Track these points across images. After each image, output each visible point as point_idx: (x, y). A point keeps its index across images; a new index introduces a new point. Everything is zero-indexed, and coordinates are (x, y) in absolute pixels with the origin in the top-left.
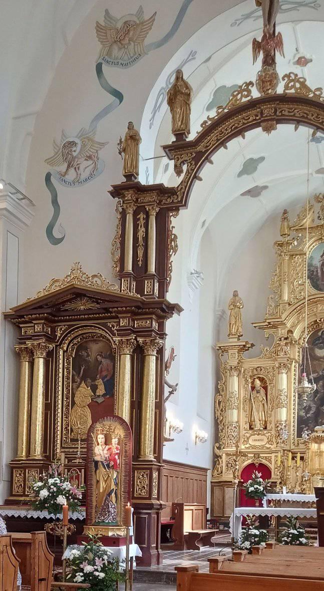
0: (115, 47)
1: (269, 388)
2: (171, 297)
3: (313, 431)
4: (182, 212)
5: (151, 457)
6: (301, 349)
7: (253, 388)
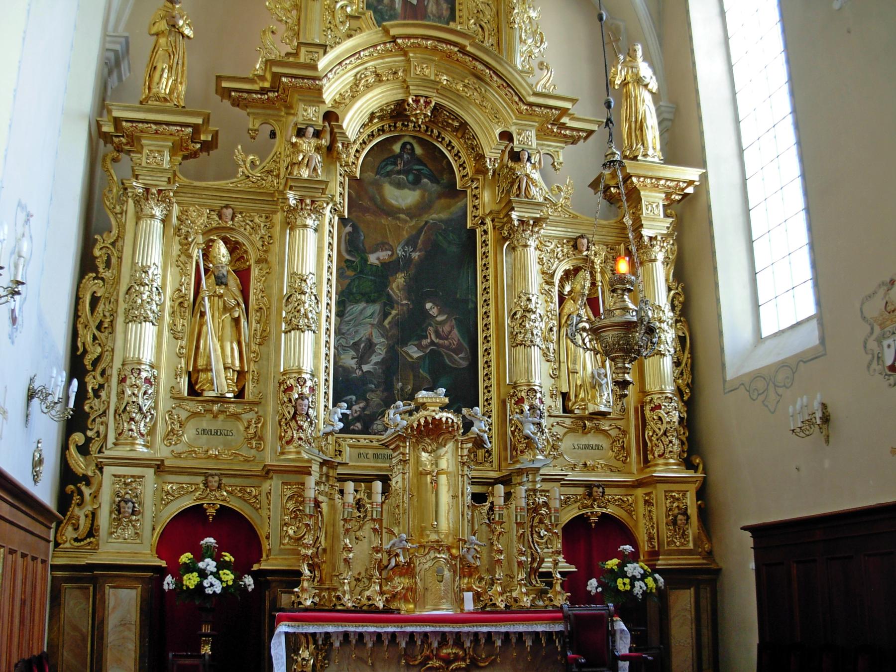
1: (255, 272)
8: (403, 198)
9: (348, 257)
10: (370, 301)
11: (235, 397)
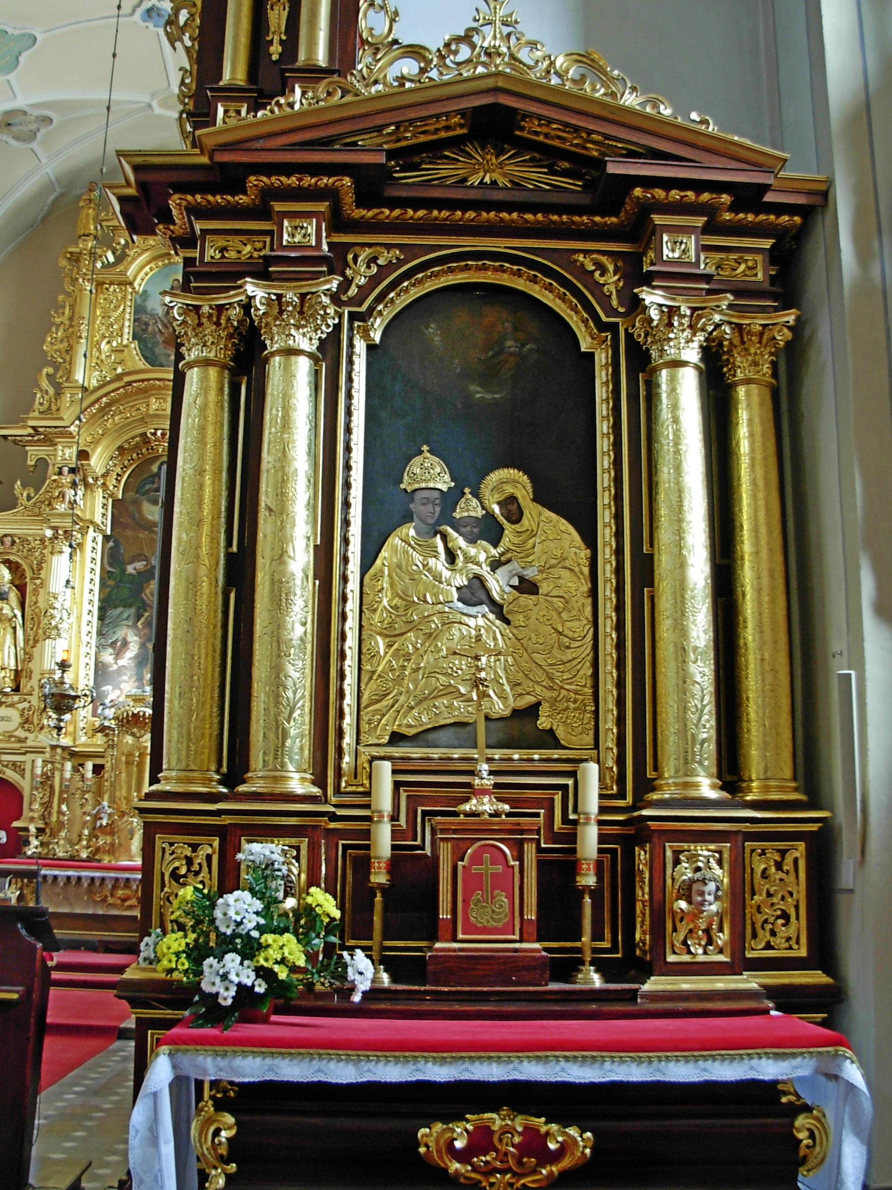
1: (29, 588)
6: (110, 500)
9: (109, 569)
10: (127, 606)
11: (12, 690)
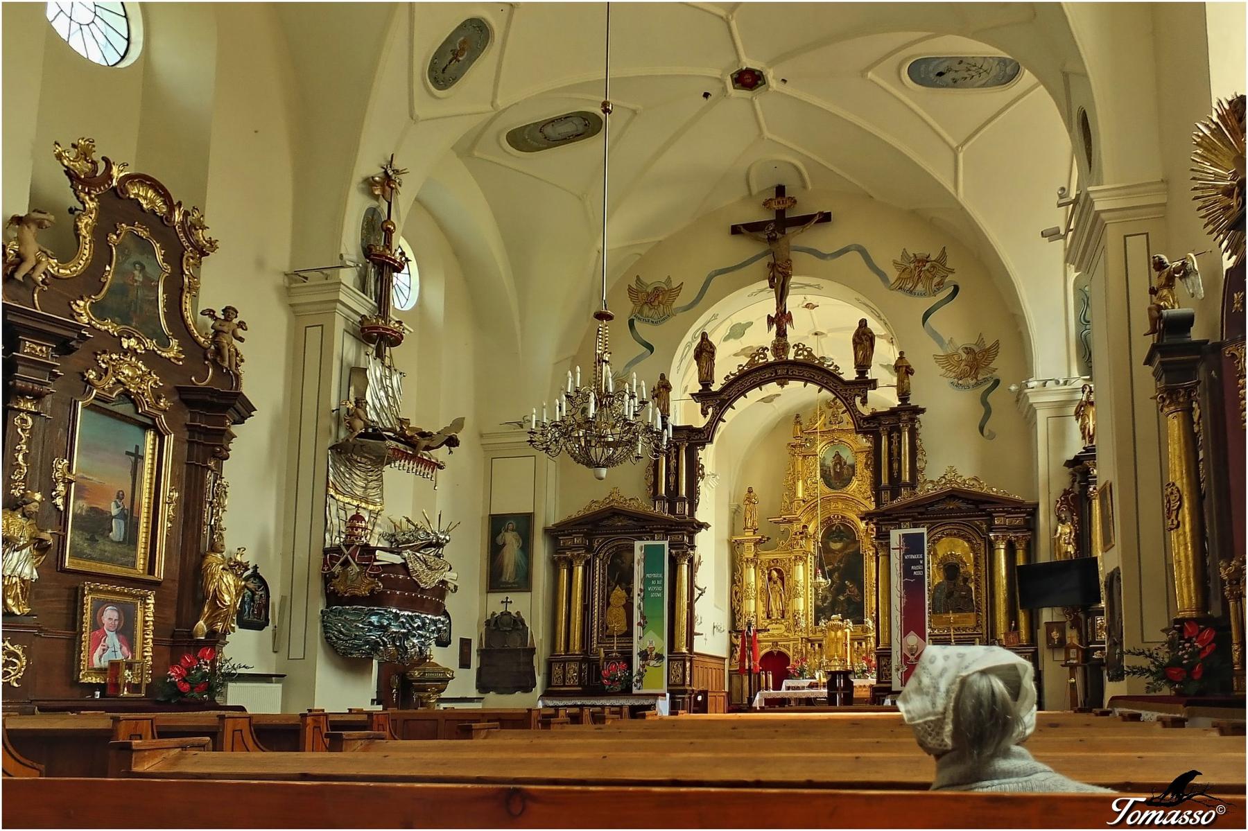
0: (646, 309)
2: (700, 516)
3: (829, 619)
4: (708, 446)
5: (684, 650)
7: (770, 579)
8: (836, 546)
